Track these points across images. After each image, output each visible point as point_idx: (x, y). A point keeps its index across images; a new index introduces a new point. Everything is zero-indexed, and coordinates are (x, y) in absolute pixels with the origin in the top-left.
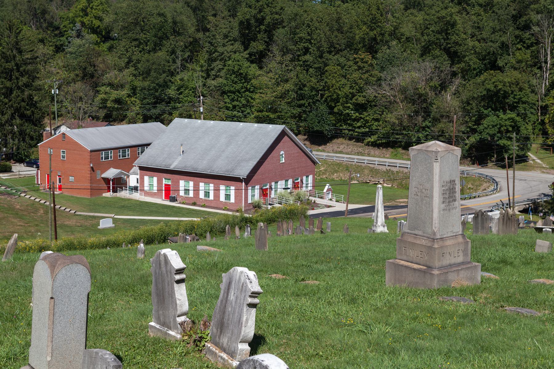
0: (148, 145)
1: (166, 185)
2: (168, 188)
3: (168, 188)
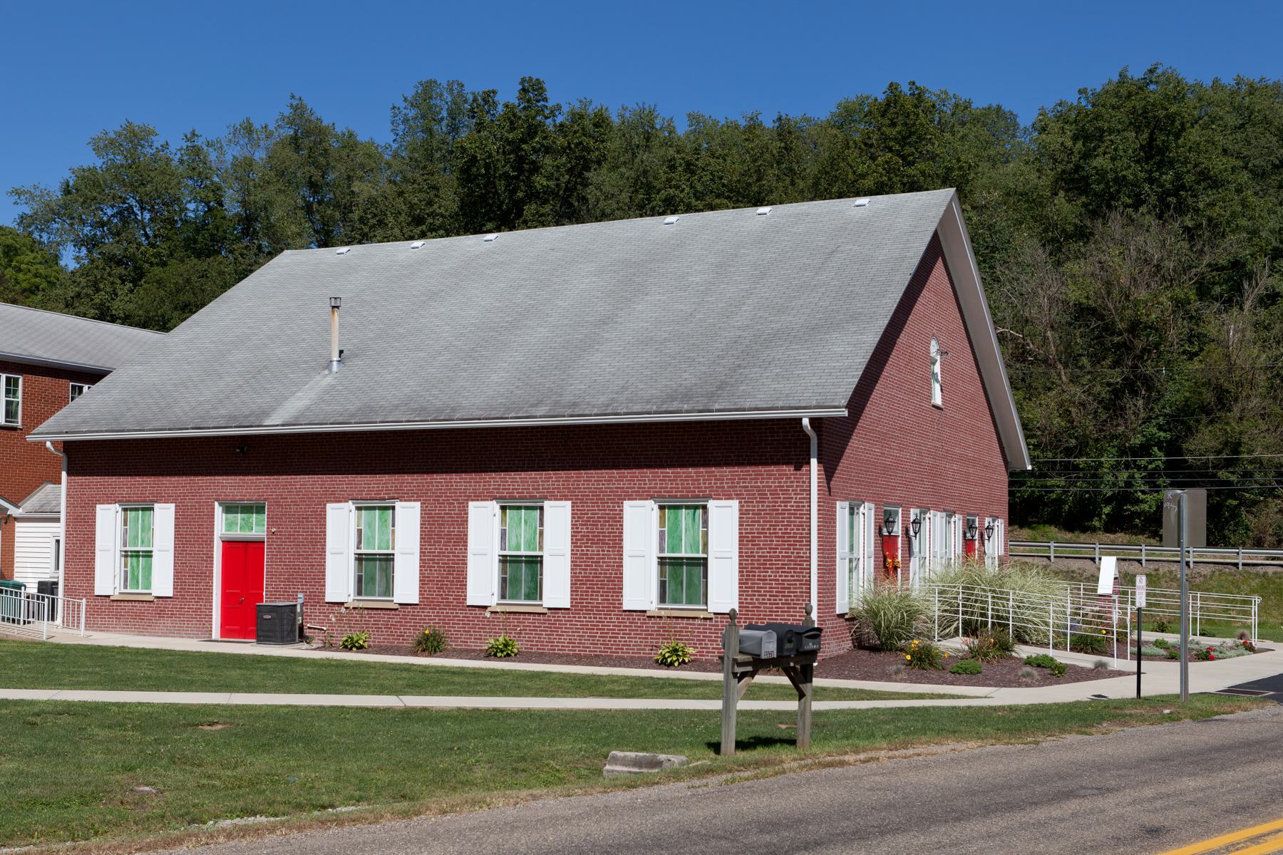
0: (94, 376)
1: (229, 545)
2: (243, 556)
3: (243, 556)
